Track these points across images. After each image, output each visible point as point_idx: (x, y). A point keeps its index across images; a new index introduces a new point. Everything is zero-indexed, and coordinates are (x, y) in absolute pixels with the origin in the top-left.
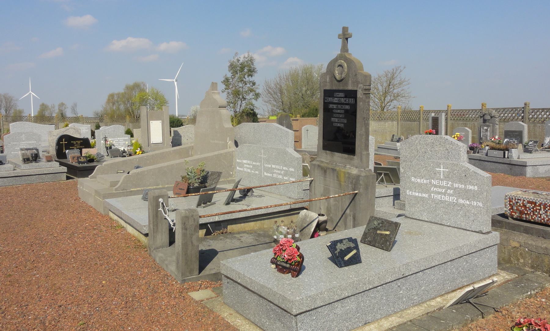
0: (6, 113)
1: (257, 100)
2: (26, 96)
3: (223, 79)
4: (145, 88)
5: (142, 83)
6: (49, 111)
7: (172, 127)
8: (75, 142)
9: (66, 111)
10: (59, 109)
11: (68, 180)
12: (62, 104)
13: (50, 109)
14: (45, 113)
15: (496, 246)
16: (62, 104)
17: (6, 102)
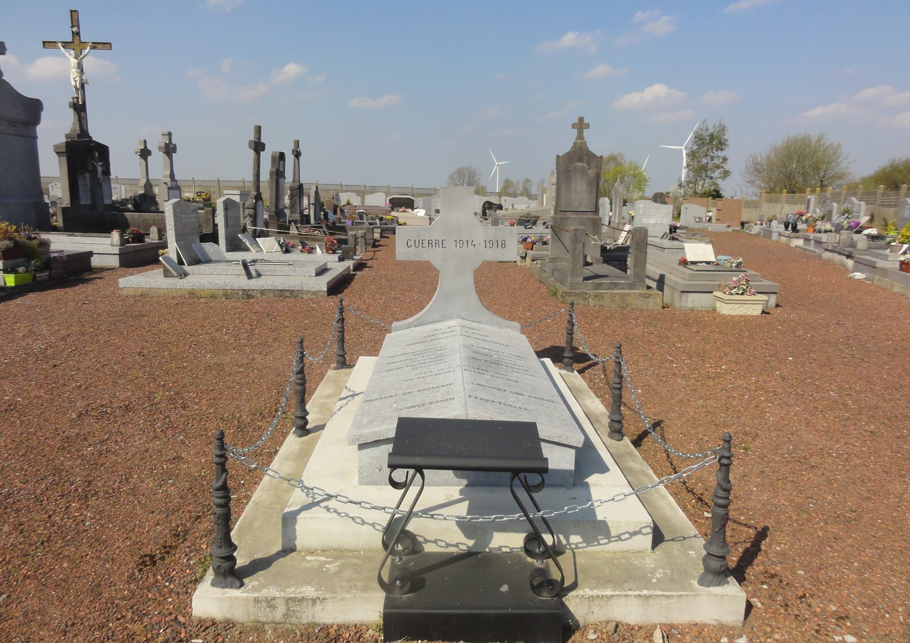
4: (623, 161)
5: (620, 155)
6: (512, 189)
10: (523, 186)
11: (218, 238)
12: (528, 181)
15: (534, 495)
16: (528, 181)
17: (469, 176)
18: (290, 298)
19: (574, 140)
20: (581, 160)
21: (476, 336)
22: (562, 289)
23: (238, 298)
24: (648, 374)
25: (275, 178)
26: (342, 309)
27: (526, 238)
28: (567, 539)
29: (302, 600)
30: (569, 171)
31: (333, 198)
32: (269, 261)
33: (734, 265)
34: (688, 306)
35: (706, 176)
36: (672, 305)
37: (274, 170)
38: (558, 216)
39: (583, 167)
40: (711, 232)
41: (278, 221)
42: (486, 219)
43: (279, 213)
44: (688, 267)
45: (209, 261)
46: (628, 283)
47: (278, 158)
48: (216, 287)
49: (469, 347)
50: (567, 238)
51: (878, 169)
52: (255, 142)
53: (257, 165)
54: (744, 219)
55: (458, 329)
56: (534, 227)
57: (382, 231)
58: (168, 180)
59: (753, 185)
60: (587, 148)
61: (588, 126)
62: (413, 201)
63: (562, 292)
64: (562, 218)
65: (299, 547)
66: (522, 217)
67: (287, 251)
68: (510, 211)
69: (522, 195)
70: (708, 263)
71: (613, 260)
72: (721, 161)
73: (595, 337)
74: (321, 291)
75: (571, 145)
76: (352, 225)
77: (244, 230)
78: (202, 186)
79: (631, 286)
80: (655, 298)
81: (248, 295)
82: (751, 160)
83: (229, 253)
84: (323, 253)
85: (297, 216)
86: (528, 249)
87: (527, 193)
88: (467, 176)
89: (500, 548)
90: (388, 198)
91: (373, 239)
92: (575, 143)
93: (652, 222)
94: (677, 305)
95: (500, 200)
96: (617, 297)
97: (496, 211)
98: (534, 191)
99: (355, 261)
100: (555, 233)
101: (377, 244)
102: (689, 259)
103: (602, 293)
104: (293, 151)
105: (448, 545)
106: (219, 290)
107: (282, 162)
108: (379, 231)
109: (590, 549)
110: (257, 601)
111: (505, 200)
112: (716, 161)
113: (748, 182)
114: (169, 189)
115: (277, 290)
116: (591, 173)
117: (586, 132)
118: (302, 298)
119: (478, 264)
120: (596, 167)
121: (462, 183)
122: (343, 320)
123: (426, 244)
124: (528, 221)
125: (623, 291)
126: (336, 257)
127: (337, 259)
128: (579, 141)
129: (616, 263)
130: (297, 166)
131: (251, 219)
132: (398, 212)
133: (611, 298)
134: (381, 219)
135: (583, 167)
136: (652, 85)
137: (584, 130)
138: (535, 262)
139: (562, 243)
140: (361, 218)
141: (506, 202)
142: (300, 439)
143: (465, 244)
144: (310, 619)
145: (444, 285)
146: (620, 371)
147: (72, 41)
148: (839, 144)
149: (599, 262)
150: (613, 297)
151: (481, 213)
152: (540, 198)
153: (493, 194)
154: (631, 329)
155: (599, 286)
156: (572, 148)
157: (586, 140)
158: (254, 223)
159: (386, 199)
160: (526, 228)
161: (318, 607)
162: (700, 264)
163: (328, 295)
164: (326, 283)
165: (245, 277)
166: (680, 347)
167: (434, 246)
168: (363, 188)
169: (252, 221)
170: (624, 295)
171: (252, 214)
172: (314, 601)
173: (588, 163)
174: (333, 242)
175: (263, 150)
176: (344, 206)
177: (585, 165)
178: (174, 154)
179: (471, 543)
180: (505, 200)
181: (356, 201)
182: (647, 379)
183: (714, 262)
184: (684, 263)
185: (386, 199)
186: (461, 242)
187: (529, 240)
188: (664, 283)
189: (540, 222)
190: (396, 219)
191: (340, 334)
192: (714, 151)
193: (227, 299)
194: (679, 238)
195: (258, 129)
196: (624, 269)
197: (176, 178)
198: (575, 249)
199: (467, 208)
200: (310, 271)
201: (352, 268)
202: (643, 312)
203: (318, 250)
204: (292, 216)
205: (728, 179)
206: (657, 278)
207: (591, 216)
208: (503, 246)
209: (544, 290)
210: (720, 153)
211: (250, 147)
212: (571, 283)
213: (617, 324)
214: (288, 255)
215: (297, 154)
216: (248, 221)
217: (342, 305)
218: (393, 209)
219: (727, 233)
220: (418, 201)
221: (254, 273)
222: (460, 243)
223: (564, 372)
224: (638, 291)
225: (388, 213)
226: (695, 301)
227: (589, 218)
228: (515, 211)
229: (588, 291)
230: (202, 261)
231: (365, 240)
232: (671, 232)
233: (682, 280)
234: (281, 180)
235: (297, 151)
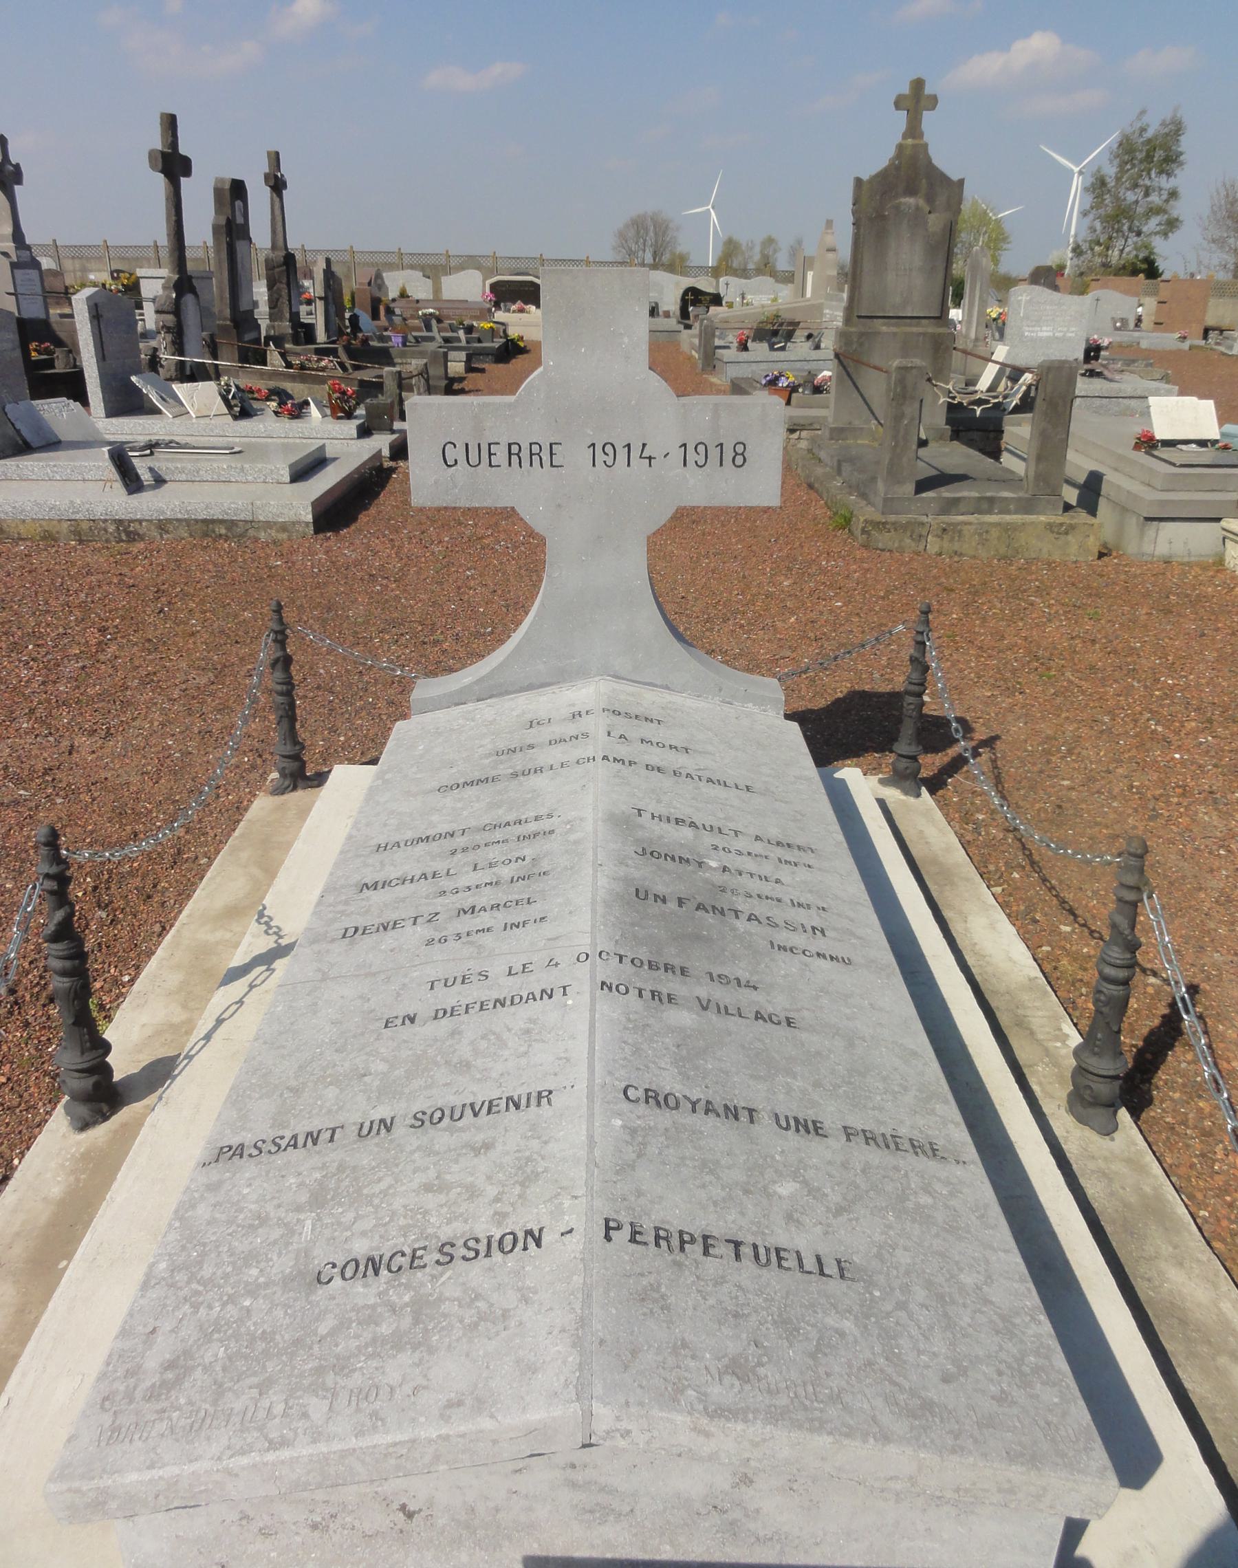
0: (654, 260)
2: (1059, 164)
6: (740, 258)
7: (200, 259)
8: (703, 298)
9: (776, 259)
12: (770, 241)
16: (770, 241)
17: (656, 234)
18: (227, 538)
19: (898, 139)
20: (911, 191)
21: (655, 756)
22: (866, 512)
23: (107, 541)
24: (1116, 791)
25: (224, 239)
26: (282, 632)
27: (777, 379)
30: (881, 217)
31: (369, 284)
32: (186, 446)
34: (1157, 553)
35: (1130, 229)
36: (1118, 548)
37: (223, 221)
38: (853, 329)
39: (918, 208)
40: (1146, 350)
41: (240, 339)
42: (688, 327)
43: (243, 320)
44: (1156, 453)
45: (53, 444)
46: (1019, 499)
47: (228, 195)
48: (53, 515)
49: (627, 880)
50: (876, 387)
52: (163, 154)
53: (173, 212)
54: (1210, 321)
55: (596, 725)
56: (789, 344)
57: (469, 358)
58: (9, 246)
59: (1222, 247)
61: (933, 101)
62: (537, 287)
63: (866, 522)
64: (862, 334)
66: (762, 322)
67: (245, 413)
68: (738, 310)
69: (759, 272)
70: (1202, 443)
71: (969, 430)
72: (1165, 197)
73: (955, 656)
74: (299, 522)
75: (891, 152)
76: (404, 344)
77: (154, 363)
78: (123, 258)
79: (1027, 506)
81: (128, 533)
82: (1223, 193)
83: (114, 420)
84: (324, 416)
85: (285, 327)
87: (766, 267)
88: (652, 234)
90: (488, 282)
91: (447, 377)
92: (900, 148)
93: (1045, 334)
94: (1131, 548)
95: (718, 282)
96: (995, 533)
97: (708, 308)
98: (782, 264)
99: (395, 436)
100: (844, 367)
101: (456, 386)
102: (1160, 435)
104: (267, 177)
106: (60, 521)
107: (238, 203)
108: (462, 355)
111: (727, 284)
112: (1155, 198)
113: (1214, 241)
114: (14, 266)
115: (196, 521)
116: (935, 222)
117: (928, 118)
118: (256, 540)
119: (663, 515)
121: (642, 247)
122: (286, 661)
123: (501, 455)
124: (775, 333)
126: (351, 427)
127: (354, 433)
128: (910, 141)
129: (976, 435)
130: (278, 212)
131: (169, 337)
132: (508, 311)
133: (980, 535)
134: (469, 330)
135: (918, 208)
136: (1027, 35)
138: (796, 435)
139: (862, 395)
140: (428, 328)
141: (729, 287)
142: (83, 1136)
143: (622, 454)
146: (1133, 927)
147: (937, 315)
150: (984, 530)
151: (678, 313)
152: (798, 278)
153: (702, 270)
154: (1037, 625)
155: (950, 506)
156: (892, 160)
157: (926, 138)
158: (179, 346)
159: (484, 285)
160: (772, 348)
162: (1183, 447)
163: (317, 531)
165: (119, 486)
166: (1172, 687)
167: (526, 462)
168: (443, 261)
169: (173, 343)
171: (171, 325)
173: (930, 199)
174: (344, 393)
175: (187, 172)
176: (394, 300)
178: (16, 187)
180: (727, 284)
181: (420, 289)
182: (1115, 810)
183: (1216, 441)
184: (1148, 443)
185: (484, 285)
186: (609, 449)
187: (783, 383)
188: (1099, 495)
189: (800, 335)
190: (502, 328)
191: (280, 699)
192: (1153, 175)
193: (81, 542)
194: (1106, 372)
195: (170, 123)
197: (28, 242)
198: (898, 418)
199: (626, 340)
201: (386, 452)
202: (1054, 569)
203: (314, 410)
204: (273, 327)
206: (1081, 479)
208: (739, 460)
209: (818, 510)
210: (1165, 183)
211: (153, 167)
212: (886, 500)
213: (1002, 610)
214: (244, 424)
215: (277, 185)
216: (162, 343)
217: (280, 620)
218: (497, 305)
221: (146, 477)
222: (603, 451)
223: (893, 795)
224: (1042, 518)
225: (486, 314)
227: (924, 334)
228: (746, 310)
229: (924, 519)
230: (34, 445)
231: (427, 380)
232: (1088, 358)
233: (1146, 488)
234: (240, 246)
235: (276, 177)
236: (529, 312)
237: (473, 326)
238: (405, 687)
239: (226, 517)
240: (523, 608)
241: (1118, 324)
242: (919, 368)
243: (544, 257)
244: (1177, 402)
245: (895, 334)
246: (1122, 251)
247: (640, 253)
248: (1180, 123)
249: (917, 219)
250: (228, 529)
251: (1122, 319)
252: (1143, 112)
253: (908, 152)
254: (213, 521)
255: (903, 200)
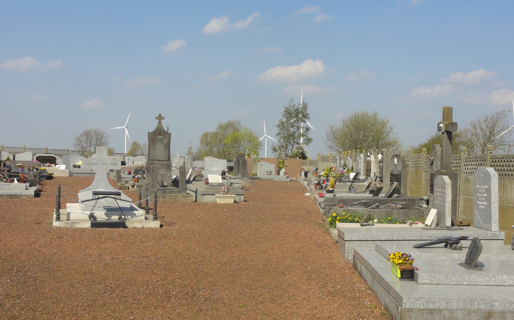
1: (308, 145)
3: (278, 123)
4: (240, 127)
5: (237, 121)
13: (141, 149)
14: (136, 153)
19: (157, 125)
20: (160, 135)
28: (127, 217)
29: (74, 223)
33: (229, 184)
35: (294, 142)
38: (149, 162)
39: (162, 138)
46: (178, 191)
51: (429, 138)
60: (164, 129)
61: (163, 118)
62: (55, 158)
65: (70, 220)
74: (31, 195)
75: (156, 127)
79: (179, 193)
80: (190, 197)
82: (330, 129)
86: (136, 182)
88: (94, 139)
89: (113, 219)
90: (35, 156)
92: (157, 126)
96: (173, 197)
103: (165, 195)
105: (102, 219)
109: (132, 219)
110: (66, 223)
111: (129, 159)
115: (9, 195)
116: (166, 141)
120: (168, 138)
123: (91, 164)
125: (175, 195)
128: (159, 125)
133: (170, 197)
137: (162, 120)
144: (76, 227)
145: (97, 177)
148: (388, 121)
149: (171, 186)
161: (78, 224)
164: (34, 191)
170: (175, 196)
172: (77, 223)
173: (164, 136)
177: (162, 137)
179: (107, 218)
180: (129, 159)
192: (299, 123)
196: (178, 187)
200: (23, 187)
205: (310, 145)
207: (166, 162)
212: (151, 191)
219: (287, 181)
220: (59, 160)
222: (103, 164)
226: (208, 199)
236: (52, 167)
237: (38, 168)
238: (79, 191)
239: (16, 194)
240: (90, 185)
241: (269, 173)
242: (156, 167)
243: (48, 148)
244: (214, 176)
245: (159, 164)
246: (292, 150)
247: (88, 148)
248: (306, 104)
249: (162, 140)
250: (16, 196)
251: (270, 171)
252: (292, 100)
253: (159, 127)
254: (13, 195)
255: (158, 137)
